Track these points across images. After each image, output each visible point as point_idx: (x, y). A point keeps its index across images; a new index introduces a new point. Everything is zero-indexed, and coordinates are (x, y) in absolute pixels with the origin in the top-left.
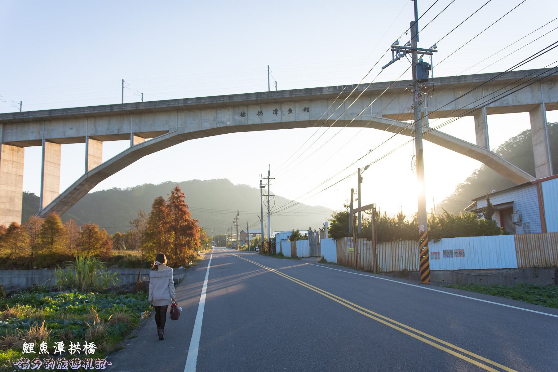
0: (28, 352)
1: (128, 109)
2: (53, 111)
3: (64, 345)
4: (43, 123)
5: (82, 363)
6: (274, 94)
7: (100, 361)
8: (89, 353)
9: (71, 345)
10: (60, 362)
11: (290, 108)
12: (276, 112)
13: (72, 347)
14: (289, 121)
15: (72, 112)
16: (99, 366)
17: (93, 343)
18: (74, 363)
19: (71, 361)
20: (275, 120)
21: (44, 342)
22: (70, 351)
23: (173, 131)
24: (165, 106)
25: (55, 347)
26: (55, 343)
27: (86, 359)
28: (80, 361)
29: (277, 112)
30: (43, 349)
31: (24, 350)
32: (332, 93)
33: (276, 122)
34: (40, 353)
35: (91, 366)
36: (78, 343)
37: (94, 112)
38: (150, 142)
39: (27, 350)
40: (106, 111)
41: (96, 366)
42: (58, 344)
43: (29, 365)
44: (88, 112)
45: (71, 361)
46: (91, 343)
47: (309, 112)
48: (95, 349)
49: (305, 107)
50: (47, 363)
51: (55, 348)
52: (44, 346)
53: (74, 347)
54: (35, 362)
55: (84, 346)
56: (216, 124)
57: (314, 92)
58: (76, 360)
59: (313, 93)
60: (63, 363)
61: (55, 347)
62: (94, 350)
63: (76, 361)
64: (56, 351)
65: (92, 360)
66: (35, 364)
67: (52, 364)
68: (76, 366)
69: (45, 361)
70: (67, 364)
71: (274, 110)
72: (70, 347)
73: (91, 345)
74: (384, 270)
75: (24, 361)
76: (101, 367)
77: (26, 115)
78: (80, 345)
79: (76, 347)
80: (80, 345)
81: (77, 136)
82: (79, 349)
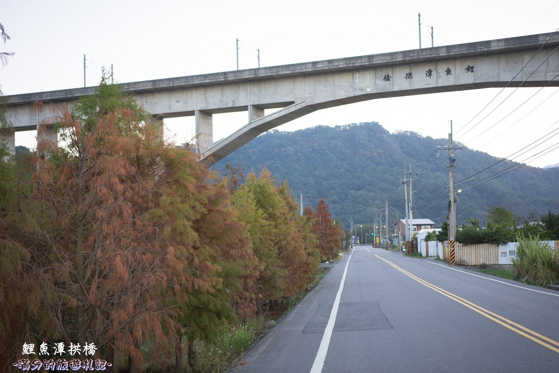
0: (28, 353)
1: (245, 77)
2: (157, 82)
3: (64, 346)
4: (145, 95)
5: (82, 364)
6: (427, 52)
7: (100, 362)
8: (90, 354)
9: (71, 346)
10: (60, 363)
11: (448, 68)
12: (429, 73)
13: (72, 348)
14: (446, 85)
15: (179, 82)
16: (99, 367)
17: (93, 344)
18: (74, 364)
19: (71, 362)
20: (429, 84)
21: (44, 343)
22: (70, 352)
23: (300, 101)
24: (290, 72)
25: (55, 348)
26: (55, 344)
27: (86, 360)
28: (80, 362)
29: (431, 73)
30: (43, 350)
31: (24, 350)
32: (504, 47)
33: (430, 86)
34: (40, 354)
35: (91, 368)
36: (78, 344)
37: (205, 82)
38: (272, 116)
39: (27, 351)
40: (219, 80)
41: (96, 367)
42: (58, 344)
43: (29, 366)
44: (198, 82)
45: (71, 362)
46: (91, 344)
47: (473, 72)
48: (95, 350)
49: (469, 66)
50: (47, 364)
51: (56, 349)
52: (44, 347)
53: (74, 348)
54: (35, 363)
55: (84, 347)
56: (353, 91)
57: (479, 47)
58: (76, 360)
59: (478, 49)
60: (63, 365)
61: (55, 348)
62: (94, 351)
63: (76, 362)
64: (56, 352)
65: (92, 361)
66: (35, 365)
67: (52, 365)
68: (76, 367)
69: (45, 362)
70: (67, 365)
71: (427, 71)
72: (70, 348)
73: (91, 346)
74: (470, 264)
75: (24, 362)
76: (101, 368)
77: (127, 87)
78: (80, 346)
79: (76, 348)
80: (80, 346)
81: (185, 110)
82: (79, 349)
